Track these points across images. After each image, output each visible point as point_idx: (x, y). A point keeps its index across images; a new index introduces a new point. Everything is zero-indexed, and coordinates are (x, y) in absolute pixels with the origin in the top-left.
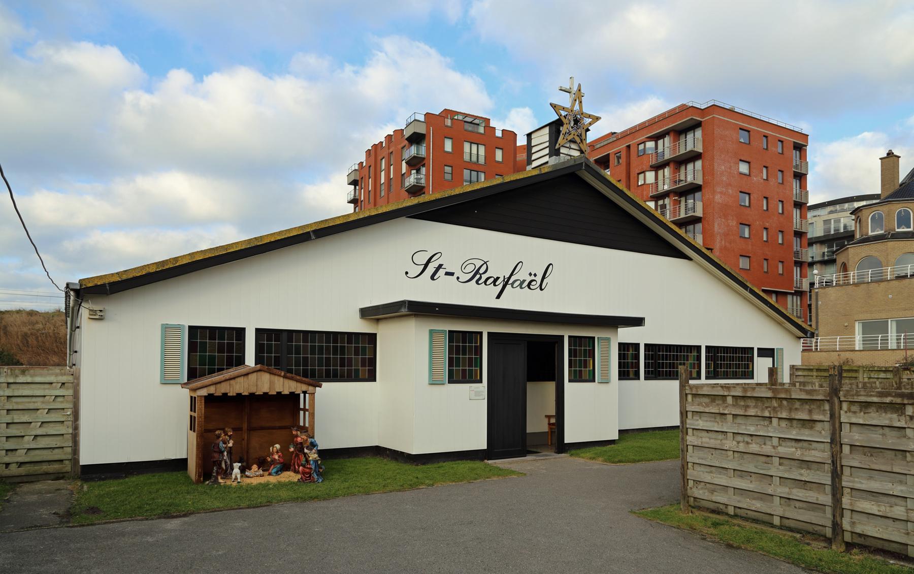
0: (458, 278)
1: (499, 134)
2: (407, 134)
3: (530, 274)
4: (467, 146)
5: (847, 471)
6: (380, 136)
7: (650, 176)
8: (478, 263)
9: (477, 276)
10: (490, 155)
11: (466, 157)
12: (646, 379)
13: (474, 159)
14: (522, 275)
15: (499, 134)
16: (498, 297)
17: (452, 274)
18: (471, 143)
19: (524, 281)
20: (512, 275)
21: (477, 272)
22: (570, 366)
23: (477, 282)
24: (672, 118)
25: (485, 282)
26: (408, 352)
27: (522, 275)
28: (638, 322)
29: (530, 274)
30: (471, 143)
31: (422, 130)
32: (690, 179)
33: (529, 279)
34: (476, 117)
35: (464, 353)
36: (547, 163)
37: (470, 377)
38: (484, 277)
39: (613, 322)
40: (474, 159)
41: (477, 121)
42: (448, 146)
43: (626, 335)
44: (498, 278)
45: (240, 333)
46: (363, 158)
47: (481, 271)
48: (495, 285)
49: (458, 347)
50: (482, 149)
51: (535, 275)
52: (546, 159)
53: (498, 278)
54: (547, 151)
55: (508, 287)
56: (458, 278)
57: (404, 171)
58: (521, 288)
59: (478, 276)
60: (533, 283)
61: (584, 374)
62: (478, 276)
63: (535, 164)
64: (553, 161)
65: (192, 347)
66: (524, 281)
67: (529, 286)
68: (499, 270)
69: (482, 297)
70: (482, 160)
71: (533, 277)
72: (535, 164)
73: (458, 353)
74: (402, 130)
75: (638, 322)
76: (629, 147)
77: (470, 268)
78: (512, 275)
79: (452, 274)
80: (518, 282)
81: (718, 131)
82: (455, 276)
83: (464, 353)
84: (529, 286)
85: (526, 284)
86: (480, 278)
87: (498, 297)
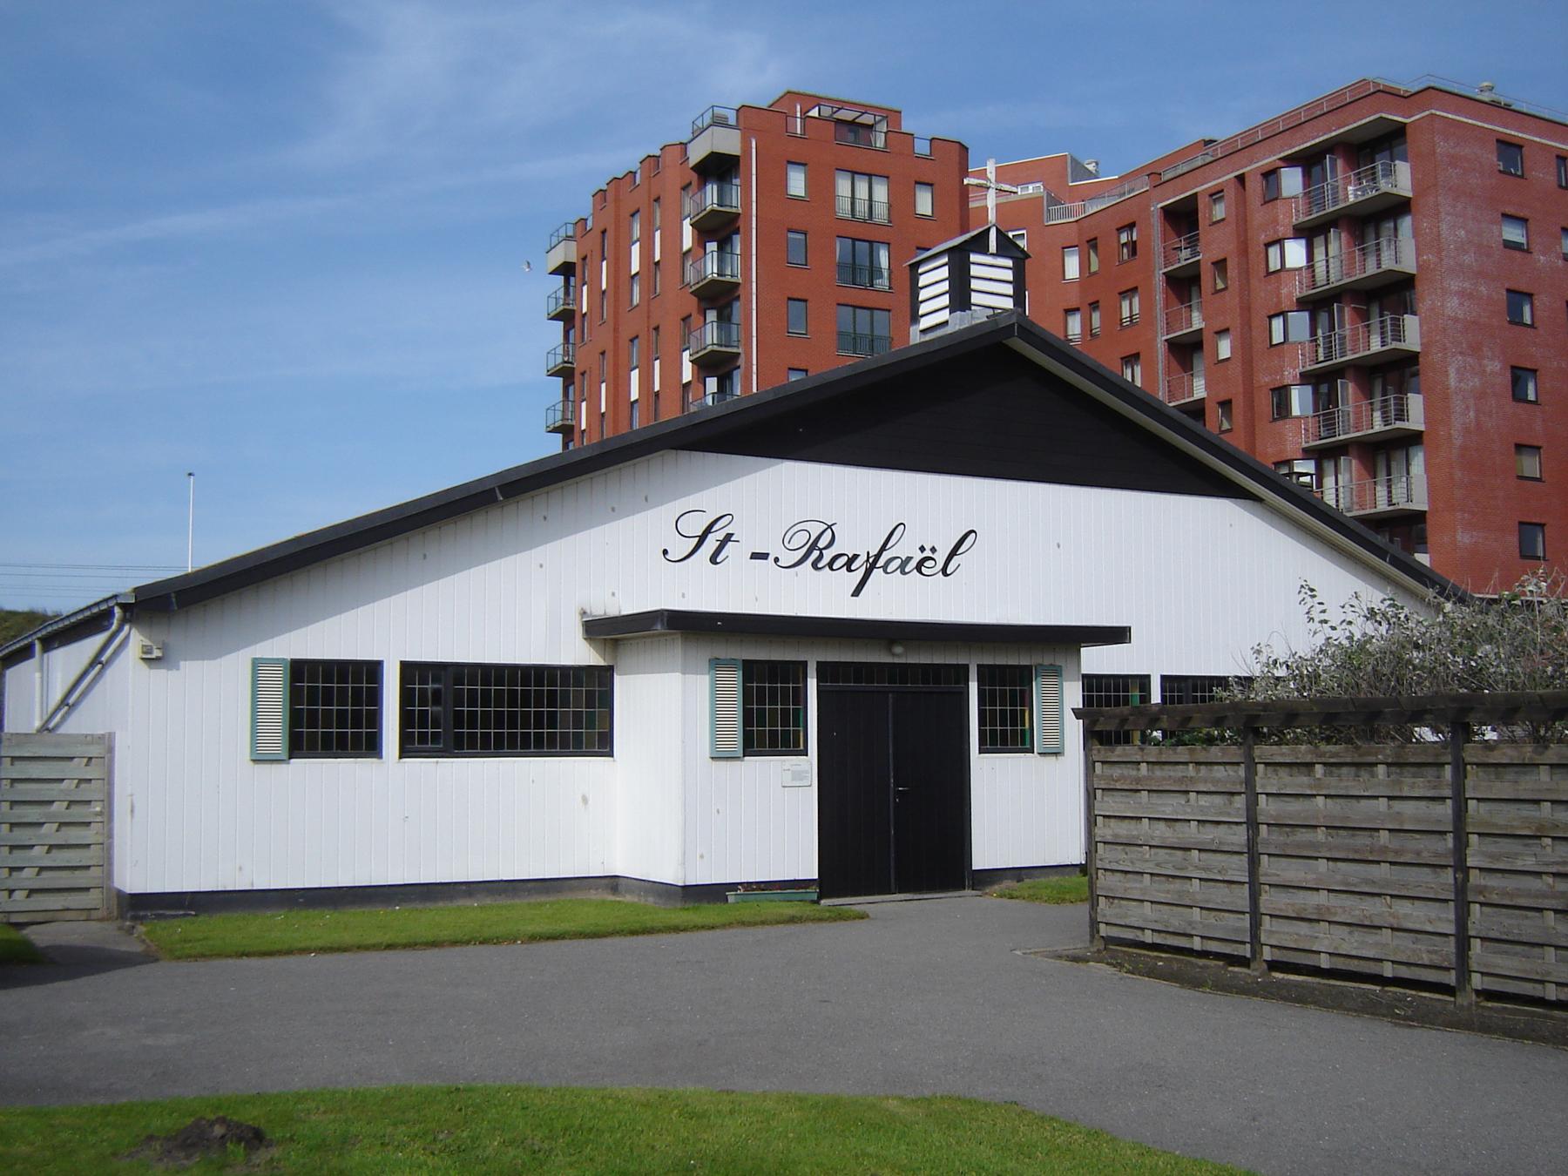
0: (776, 560)
1: (922, 148)
2: (696, 154)
3: (922, 549)
4: (843, 186)
5: (1264, 859)
6: (627, 159)
7: (1295, 253)
8: (816, 529)
9: (815, 553)
10: (901, 202)
11: (843, 208)
12: (405, 752)
13: (862, 209)
14: (898, 550)
15: (922, 148)
16: (856, 593)
17: (764, 556)
18: (854, 173)
19: (909, 559)
20: (883, 549)
21: (814, 546)
22: (982, 722)
23: (815, 565)
24: (1320, 122)
25: (830, 565)
26: (667, 710)
27: (905, 547)
28: (1118, 635)
29: (922, 549)
30: (854, 173)
31: (728, 142)
32: (1387, 263)
33: (918, 556)
34: (865, 109)
35: (773, 701)
36: (946, 323)
37: (790, 745)
38: (828, 555)
39: (1068, 639)
40: (862, 209)
41: (867, 119)
42: (797, 183)
43: (1097, 660)
44: (856, 556)
45: (373, 670)
46: (585, 207)
47: (821, 544)
48: (849, 570)
49: (761, 690)
50: (881, 192)
51: (933, 550)
52: (944, 315)
53: (856, 556)
54: (945, 300)
55: (877, 573)
56: (776, 560)
57: (687, 243)
58: (903, 573)
59: (816, 554)
60: (929, 563)
61: (1009, 733)
62: (816, 554)
63: (925, 323)
64: (960, 322)
65: (295, 695)
66: (909, 559)
67: (919, 568)
68: (858, 540)
69: (824, 596)
70: (881, 212)
71: (928, 553)
72: (925, 323)
73: (761, 701)
74: (684, 145)
75: (1118, 635)
76: (1241, 179)
77: (801, 539)
78: (883, 549)
79: (764, 556)
80: (898, 562)
81: (1442, 147)
82: (771, 558)
83: (773, 701)
84: (919, 568)
85: (913, 564)
86: (821, 556)
87: (856, 593)
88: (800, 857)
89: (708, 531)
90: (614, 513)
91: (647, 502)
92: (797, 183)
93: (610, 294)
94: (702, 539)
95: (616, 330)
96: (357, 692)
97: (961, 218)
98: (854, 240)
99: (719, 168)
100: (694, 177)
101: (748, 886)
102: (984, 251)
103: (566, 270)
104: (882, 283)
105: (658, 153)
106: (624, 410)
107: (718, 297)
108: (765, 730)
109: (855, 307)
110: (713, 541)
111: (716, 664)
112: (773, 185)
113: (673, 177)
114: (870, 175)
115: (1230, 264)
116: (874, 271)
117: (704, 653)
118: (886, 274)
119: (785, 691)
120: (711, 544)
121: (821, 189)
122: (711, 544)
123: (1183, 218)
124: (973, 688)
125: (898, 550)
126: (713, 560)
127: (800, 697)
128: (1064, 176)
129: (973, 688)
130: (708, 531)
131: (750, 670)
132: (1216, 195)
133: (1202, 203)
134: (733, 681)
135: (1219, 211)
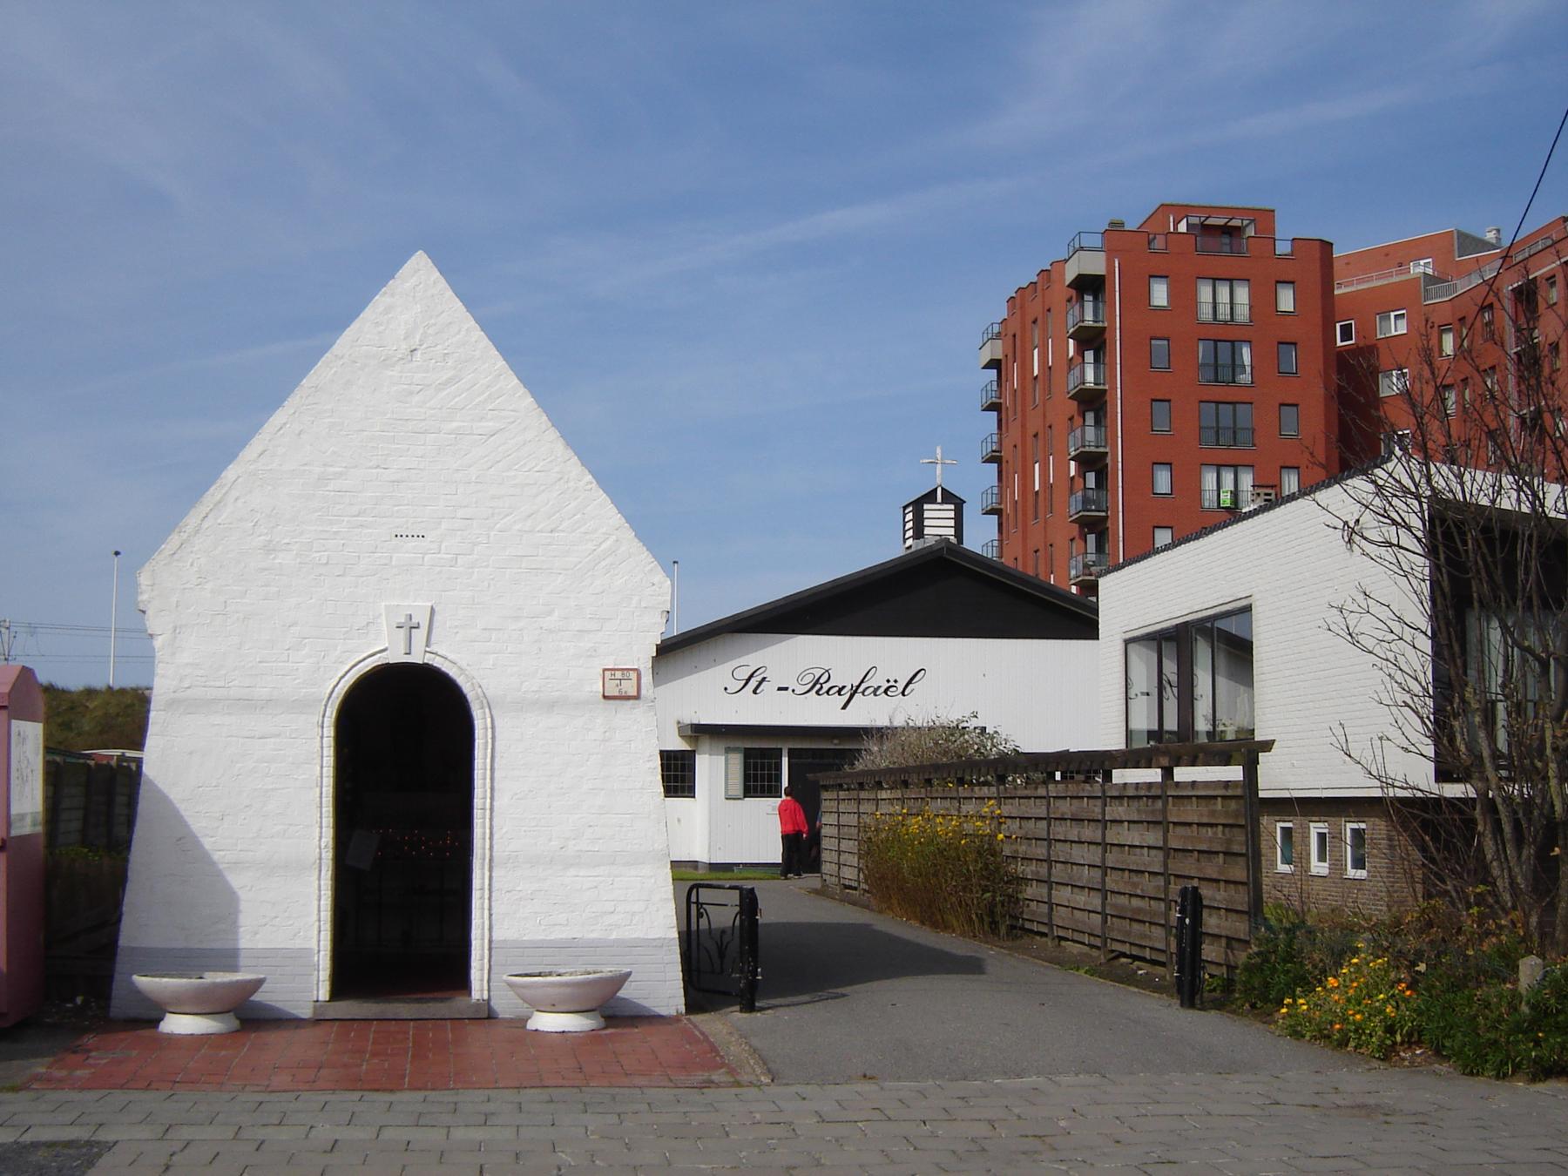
2: (1070, 276)
4: (1205, 292)
10: (1263, 302)
11: (1206, 313)
14: (872, 682)
15: (1283, 248)
27: (877, 680)
31: (1094, 264)
38: (826, 687)
42: (1160, 294)
49: (755, 764)
50: (1242, 294)
68: (845, 676)
70: (1243, 313)
77: (809, 678)
88: (773, 853)
89: (752, 676)
90: (696, 669)
91: (715, 663)
92: (1160, 294)
93: (1019, 393)
94: (748, 681)
95: (1023, 426)
96: (770, 776)
97: (1324, 309)
98: (1216, 341)
99: (1089, 286)
100: (1073, 293)
101: (745, 864)
102: (934, 501)
103: (994, 364)
104: (1245, 378)
105: (1035, 279)
106: (1031, 498)
107: (1092, 402)
108: (757, 782)
109: (1217, 403)
110: (755, 682)
111: (728, 750)
112: (1137, 296)
113: (1061, 292)
114: (1231, 280)
115: (1562, 346)
116: (1235, 366)
117: (722, 746)
118: (1248, 369)
119: (770, 765)
120: (753, 683)
121: (1183, 298)
122: (753, 683)
123: (1527, 296)
124: (785, 761)
125: (872, 682)
126: (755, 692)
127: (779, 767)
128: (1451, 252)
129: (785, 761)
130: (752, 676)
131: (748, 754)
132: (1551, 279)
133: (1543, 285)
134: (737, 761)
135: (1554, 295)
